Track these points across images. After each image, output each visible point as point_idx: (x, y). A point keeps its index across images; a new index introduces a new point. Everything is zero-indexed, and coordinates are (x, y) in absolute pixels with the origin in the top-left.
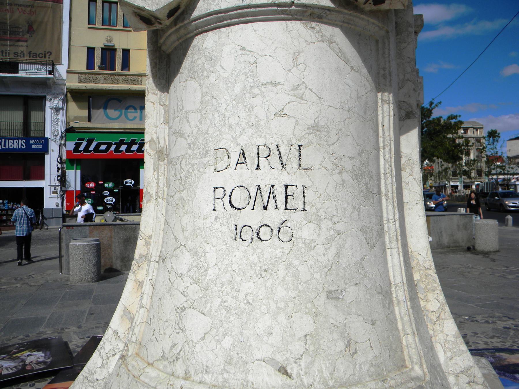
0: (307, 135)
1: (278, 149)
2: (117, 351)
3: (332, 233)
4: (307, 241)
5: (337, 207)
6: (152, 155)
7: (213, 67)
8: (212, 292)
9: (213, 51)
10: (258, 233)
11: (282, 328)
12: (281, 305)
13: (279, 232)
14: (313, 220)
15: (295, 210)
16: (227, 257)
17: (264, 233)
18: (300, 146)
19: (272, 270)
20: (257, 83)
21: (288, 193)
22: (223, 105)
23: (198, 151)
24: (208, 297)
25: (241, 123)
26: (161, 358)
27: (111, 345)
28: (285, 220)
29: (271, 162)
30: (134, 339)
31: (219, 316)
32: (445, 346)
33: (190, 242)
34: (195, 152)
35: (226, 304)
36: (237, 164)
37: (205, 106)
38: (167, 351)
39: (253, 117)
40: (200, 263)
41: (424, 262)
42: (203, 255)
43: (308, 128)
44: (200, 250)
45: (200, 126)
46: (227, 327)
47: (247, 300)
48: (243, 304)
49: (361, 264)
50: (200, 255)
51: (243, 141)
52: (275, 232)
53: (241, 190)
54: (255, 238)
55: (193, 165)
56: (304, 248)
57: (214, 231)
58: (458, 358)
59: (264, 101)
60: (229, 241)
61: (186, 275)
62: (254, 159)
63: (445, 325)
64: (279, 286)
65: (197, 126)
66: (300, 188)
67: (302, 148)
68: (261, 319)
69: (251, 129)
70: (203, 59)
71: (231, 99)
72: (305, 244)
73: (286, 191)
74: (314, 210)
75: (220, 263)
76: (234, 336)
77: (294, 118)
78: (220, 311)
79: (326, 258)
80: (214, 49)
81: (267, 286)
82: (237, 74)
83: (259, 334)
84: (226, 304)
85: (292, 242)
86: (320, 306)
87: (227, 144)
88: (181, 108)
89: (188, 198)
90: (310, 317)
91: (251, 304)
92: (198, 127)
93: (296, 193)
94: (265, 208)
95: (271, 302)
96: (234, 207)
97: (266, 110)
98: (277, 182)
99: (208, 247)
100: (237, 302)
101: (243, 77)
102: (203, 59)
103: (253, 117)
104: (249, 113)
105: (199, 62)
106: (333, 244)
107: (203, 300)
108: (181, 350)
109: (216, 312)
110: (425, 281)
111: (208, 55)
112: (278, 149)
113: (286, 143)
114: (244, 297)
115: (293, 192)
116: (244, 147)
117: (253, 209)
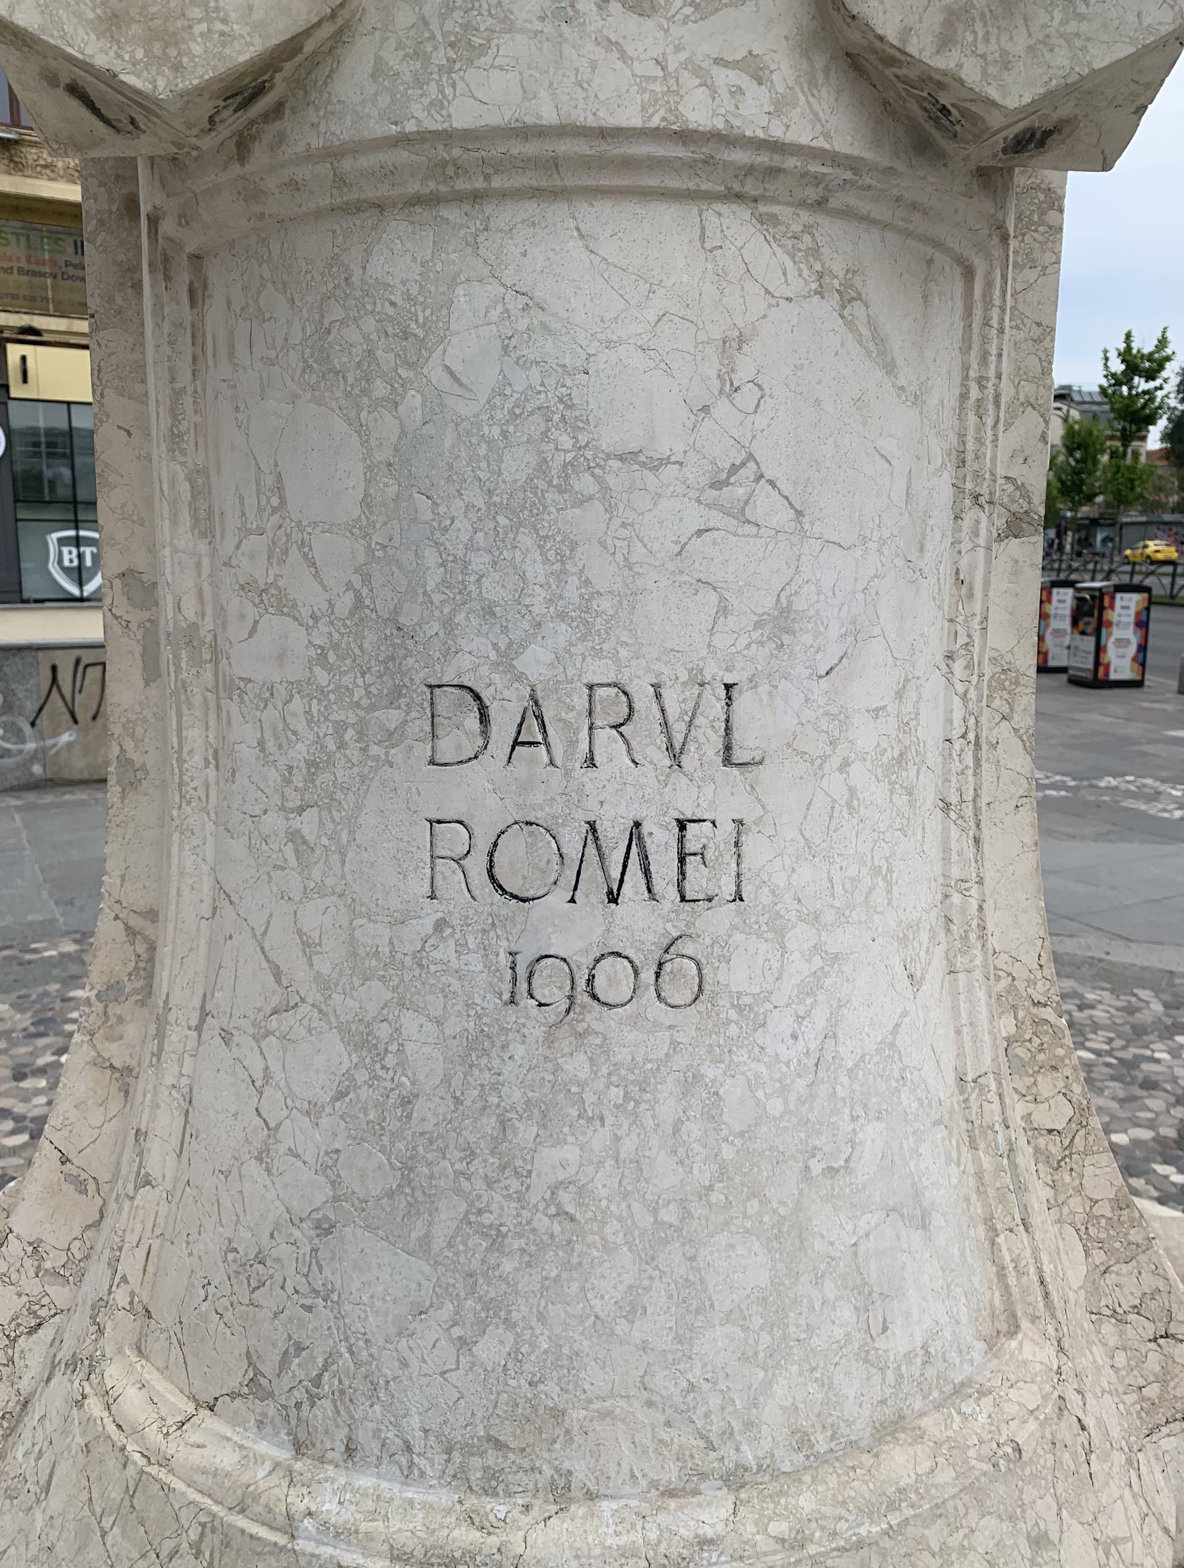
0: (754, 646)
1: (658, 696)
2: (43, 1312)
3: (817, 962)
4: (747, 1000)
5: (831, 880)
6: (133, 626)
7: (411, 366)
8: (432, 1177)
9: (409, 298)
10: (591, 980)
11: (672, 1286)
12: (670, 1215)
13: (658, 975)
14: (764, 928)
15: (710, 900)
16: (484, 1061)
17: (614, 980)
18: (728, 687)
19: (637, 1103)
20: (589, 454)
21: (690, 847)
22: (457, 524)
23: (360, 681)
24: (418, 1194)
25: (527, 601)
26: (245, 1390)
27: (19, 1295)
28: (676, 934)
29: (633, 743)
30: (121, 1297)
31: (462, 1259)
32: (1087, 1233)
33: (337, 998)
34: (346, 680)
35: (487, 1219)
36: (516, 743)
37: (382, 519)
38: (268, 1368)
39: (574, 581)
40: (380, 1073)
41: (1031, 983)
42: (394, 1047)
43: (758, 625)
44: (383, 1031)
45: (365, 592)
46: (492, 1295)
47: (559, 1206)
48: (546, 1220)
49: (892, 1045)
50: (381, 1047)
51: (536, 662)
52: (648, 976)
53: (531, 834)
54: (583, 998)
55: (340, 728)
56: (737, 1023)
57: (433, 968)
58: (1125, 1268)
59: (613, 527)
60: (491, 1007)
61: (328, 1109)
62: (577, 731)
63: (1088, 1171)
64: (662, 1153)
65: (349, 586)
66: (727, 828)
67: (735, 693)
68: (607, 1265)
69: (564, 626)
70: (369, 324)
71: (489, 504)
72: (740, 1009)
73: (681, 840)
74: (765, 898)
75: (457, 1081)
76: (515, 1325)
77: (715, 589)
78: (465, 1244)
79: (800, 1046)
80: (414, 290)
81: (623, 1155)
82: (511, 412)
83: (602, 1316)
84: (487, 1219)
85: (700, 1006)
86: (784, 1204)
87: (475, 670)
88: (275, 501)
89: (325, 841)
90: (757, 1244)
91: (572, 1219)
92: (357, 593)
93: (711, 845)
94: (613, 898)
95: (636, 1207)
96: (504, 891)
97: (619, 557)
98: (653, 811)
99: (409, 1021)
100: (524, 1213)
101: (535, 425)
102: (369, 324)
103: (574, 581)
104: (557, 567)
105: (352, 334)
106: (820, 998)
107: (402, 1201)
108: (325, 1368)
109: (450, 1245)
110: (1030, 1041)
111: (391, 311)
112: (658, 696)
113: (684, 677)
114: (548, 1195)
115: (704, 841)
116: (539, 688)
117: (572, 901)
